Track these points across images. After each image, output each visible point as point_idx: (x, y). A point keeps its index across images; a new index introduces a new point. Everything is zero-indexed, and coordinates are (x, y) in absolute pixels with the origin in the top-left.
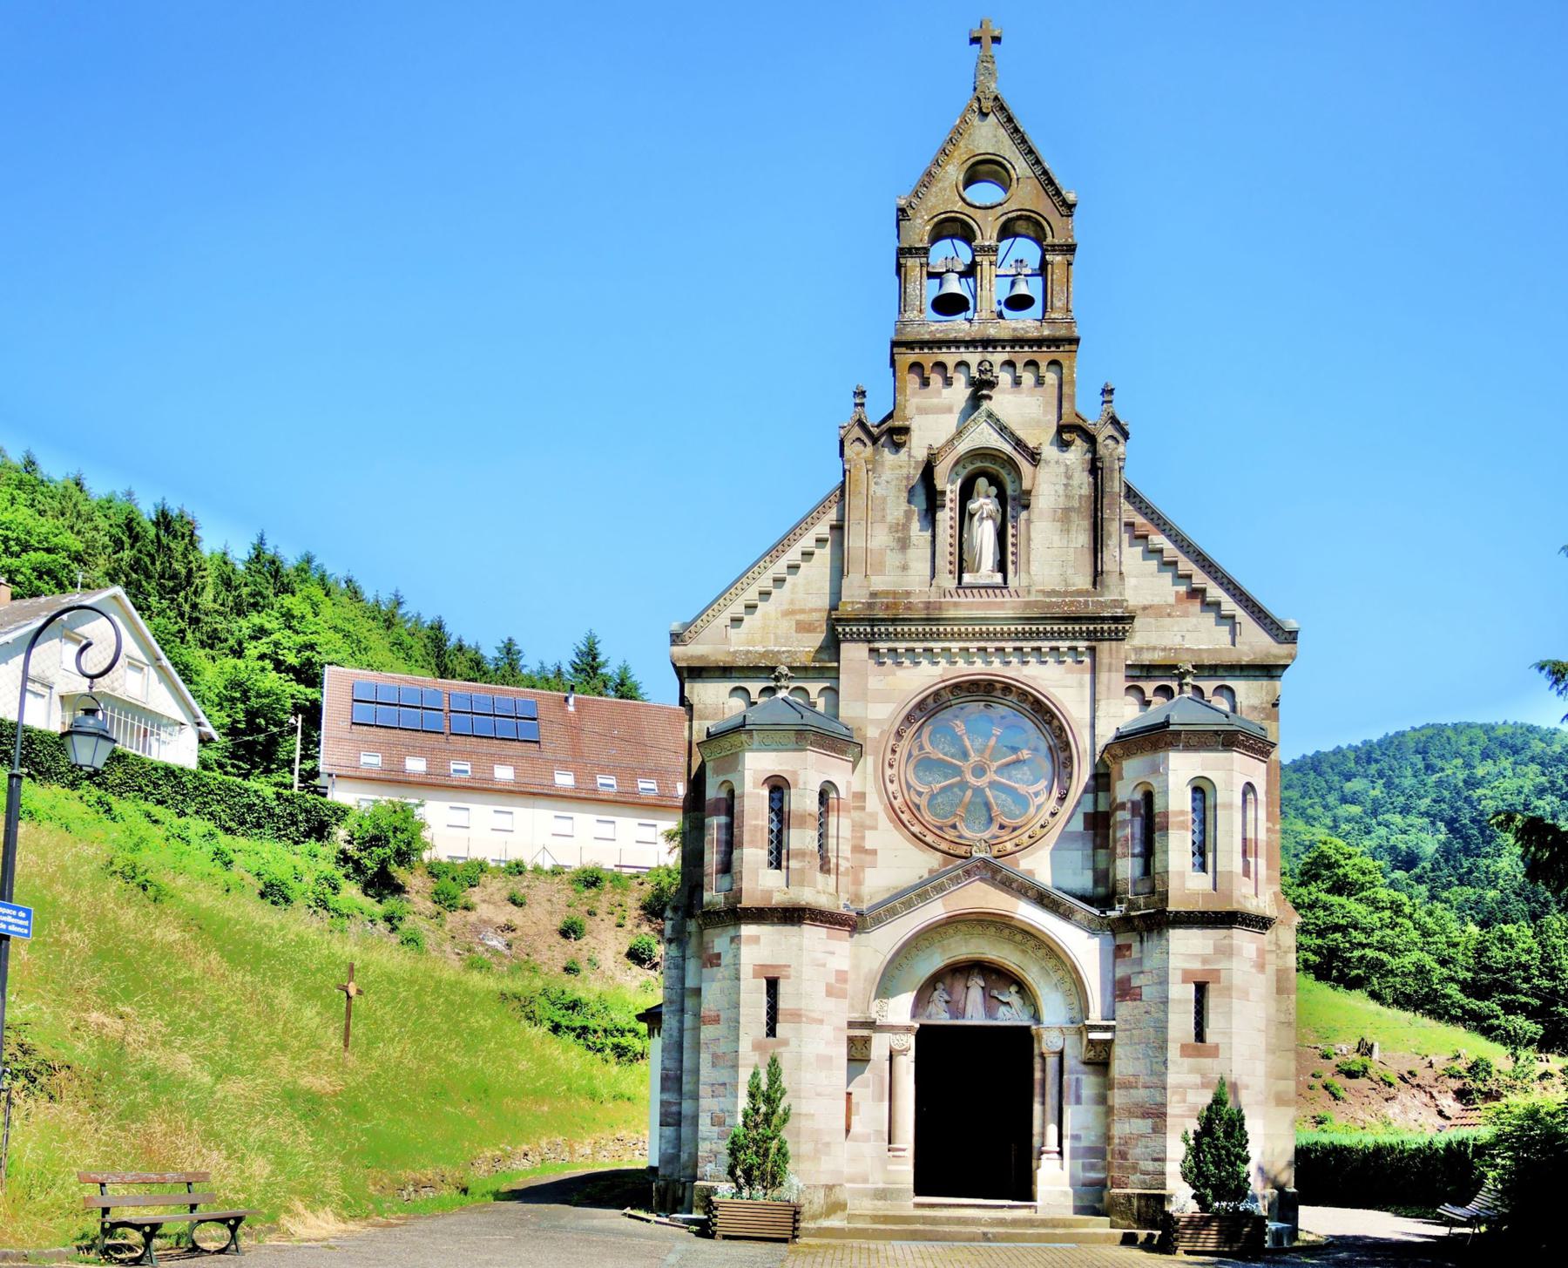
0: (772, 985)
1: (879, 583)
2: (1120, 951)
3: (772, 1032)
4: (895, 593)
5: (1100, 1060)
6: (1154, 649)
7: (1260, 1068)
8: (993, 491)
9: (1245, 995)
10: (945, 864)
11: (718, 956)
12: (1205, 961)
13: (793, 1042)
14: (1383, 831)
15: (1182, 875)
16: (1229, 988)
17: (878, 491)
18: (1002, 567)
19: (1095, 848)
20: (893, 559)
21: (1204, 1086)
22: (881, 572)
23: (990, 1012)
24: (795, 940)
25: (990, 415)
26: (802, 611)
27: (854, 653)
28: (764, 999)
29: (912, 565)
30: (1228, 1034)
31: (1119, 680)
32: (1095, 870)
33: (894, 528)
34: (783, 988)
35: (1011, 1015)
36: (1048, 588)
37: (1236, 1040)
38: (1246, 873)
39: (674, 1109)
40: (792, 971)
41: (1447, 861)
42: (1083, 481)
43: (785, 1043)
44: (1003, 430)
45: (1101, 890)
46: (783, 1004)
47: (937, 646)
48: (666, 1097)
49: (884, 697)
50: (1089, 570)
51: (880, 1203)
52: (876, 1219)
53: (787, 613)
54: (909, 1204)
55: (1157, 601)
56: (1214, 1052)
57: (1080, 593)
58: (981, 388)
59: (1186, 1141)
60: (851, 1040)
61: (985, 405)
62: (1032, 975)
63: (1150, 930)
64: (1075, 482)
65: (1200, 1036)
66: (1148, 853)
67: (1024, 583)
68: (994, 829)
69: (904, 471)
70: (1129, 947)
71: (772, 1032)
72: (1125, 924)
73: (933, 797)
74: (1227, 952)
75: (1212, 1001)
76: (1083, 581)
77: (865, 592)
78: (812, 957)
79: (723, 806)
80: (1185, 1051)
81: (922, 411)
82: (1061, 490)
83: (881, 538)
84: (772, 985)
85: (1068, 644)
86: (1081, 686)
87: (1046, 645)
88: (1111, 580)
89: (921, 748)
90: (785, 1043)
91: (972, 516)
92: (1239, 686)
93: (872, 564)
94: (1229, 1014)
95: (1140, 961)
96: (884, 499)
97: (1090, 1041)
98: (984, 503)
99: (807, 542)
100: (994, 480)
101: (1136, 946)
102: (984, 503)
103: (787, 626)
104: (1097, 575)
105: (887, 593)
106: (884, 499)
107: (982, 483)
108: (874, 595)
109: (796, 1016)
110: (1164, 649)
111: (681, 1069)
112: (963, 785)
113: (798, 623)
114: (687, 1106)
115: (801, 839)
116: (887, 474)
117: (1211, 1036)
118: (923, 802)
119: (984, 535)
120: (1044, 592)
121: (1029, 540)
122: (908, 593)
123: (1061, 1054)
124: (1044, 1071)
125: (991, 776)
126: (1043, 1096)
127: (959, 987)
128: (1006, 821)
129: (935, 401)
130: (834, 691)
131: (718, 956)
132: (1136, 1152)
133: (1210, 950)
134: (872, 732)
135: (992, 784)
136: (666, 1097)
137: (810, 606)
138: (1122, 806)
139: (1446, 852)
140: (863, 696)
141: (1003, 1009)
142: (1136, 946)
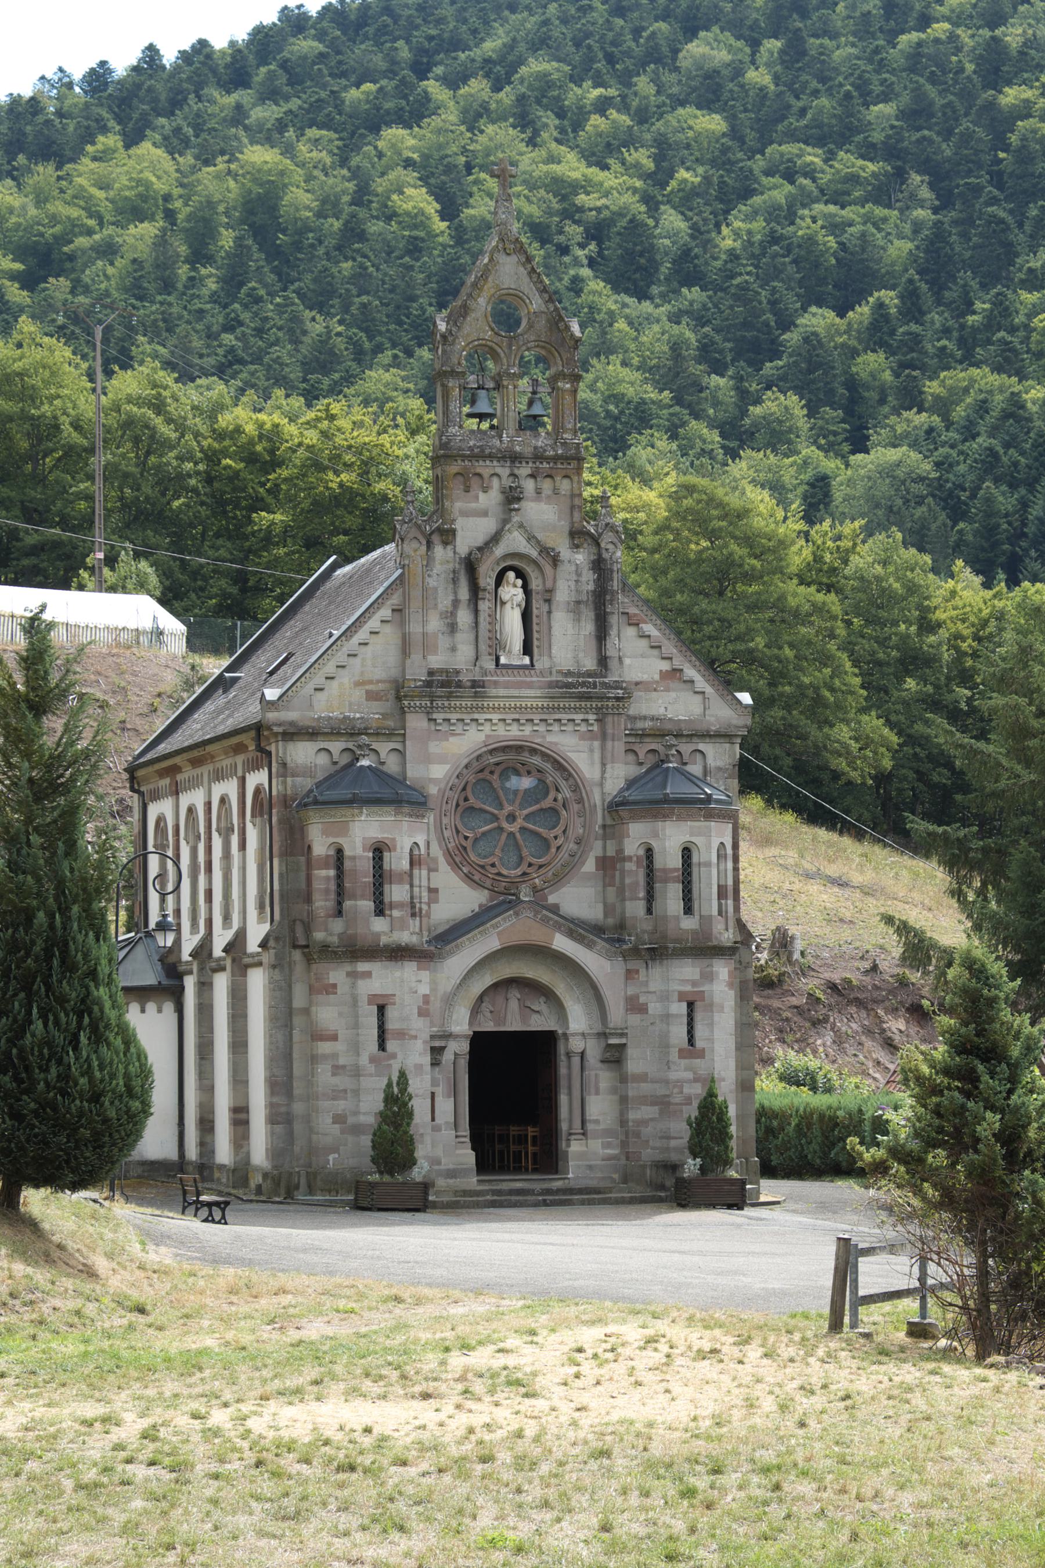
0: (381, 1009)
1: (437, 661)
2: (630, 974)
3: (382, 1046)
4: (447, 671)
5: (615, 1057)
6: (645, 718)
7: (732, 1063)
8: (519, 582)
9: (721, 1009)
10: (491, 899)
11: (335, 986)
12: (694, 984)
13: (400, 1056)
14: (779, 192)
15: (677, 918)
16: (711, 1005)
17: (432, 582)
18: (527, 649)
19: (605, 886)
20: (443, 642)
21: (696, 1080)
22: (435, 653)
23: (524, 1019)
24: (398, 974)
25: (521, 526)
26: (370, 682)
27: (416, 723)
28: (374, 1021)
29: (459, 646)
30: (711, 1040)
31: (620, 746)
32: (605, 905)
33: (444, 615)
34: (391, 1013)
35: (540, 1022)
36: (565, 669)
37: (716, 1046)
38: (720, 913)
39: (283, 1109)
40: (397, 999)
41: (938, 287)
42: (589, 578)
43: (394, 1056)
44: (531, 538)
45: (610, 921)
46: (391, 1025)
47: (481, 717)
48: (275, 1100)
49: (442, 760)
50: (594, 653)
51: (451, 1181)
52: (456, 1193)
53: (358, 684)
54: (472, 1182)
55: (645, 677)
56: (701, 1054)
57: (589, 674)
58: (512, 498)
59: (690, 1124)
60: (433, 1049)
61: (516, 519)
62: (561, 989)
63: (653, 959)
64: (584, 579)
65: (691, 1041)
66: (650, 897)
67: (547, 665)
68: (524, 867)
69: (451, 566)
70: (637, 972)
71: (382, 1046)
72: (635, 952)
73: (476, 840)
74: (708, 977)
75: (698, 1016)
76: (590, 664)
77: (425, 671)
78: (405, 984)
79: (332, 861)
80: (682, 1054)
81: (466, 514)
82: (572, 584)
83: (435, 624)
84: (381, 1009)
85: (581, 716)
86: (591, 751)
87: (564, 717)
88: (613, 664)
89: (466, 799)
90: (394, 1056)
91: (503, 603)
92: (708, 748)
93: (428, 646)
94: (711, 1025)
95: (646, 984)
96: (436, 589)
97: (609, 1046)
98: (512, 592)
99: (373, 623)
100: (520, 574)
101: (643, 972)
102: (512, 592)
103: (359, 694)
104: (603, 661)
105: (441, 671)
106: (436, 589)
107: (511, 575)
108: (431, 673)
109: (401, 1035)
110: (652, 719)
111: (290, 1076)
112: (501, 829)
113: (367, 692)
114: (298, 1108)
115: (396, 893)
116: (438, 568)
117: (699, 1044)
118: (468, 844)
119: (512, 622)
120: (559, 672)
121: (550, 628)
122: (457, 672)
123: (582, 1054)
124: (569, 1067)
125: (520, 822)
126: (570, 1088)
127: (500, 999)
128: (534, 860)
129: (474, 505)
130: (401, 753)
131: (335, 986)
132: (647, 1131)
133: (697, 977)
134: (433, 790)
135: (523, 829)
136: (275, 1100)
137: (376, 677)
138: (630, 858)
139: (935, 263)
140: (428, 759)
141: (535, 1016)
142: (643, 972)
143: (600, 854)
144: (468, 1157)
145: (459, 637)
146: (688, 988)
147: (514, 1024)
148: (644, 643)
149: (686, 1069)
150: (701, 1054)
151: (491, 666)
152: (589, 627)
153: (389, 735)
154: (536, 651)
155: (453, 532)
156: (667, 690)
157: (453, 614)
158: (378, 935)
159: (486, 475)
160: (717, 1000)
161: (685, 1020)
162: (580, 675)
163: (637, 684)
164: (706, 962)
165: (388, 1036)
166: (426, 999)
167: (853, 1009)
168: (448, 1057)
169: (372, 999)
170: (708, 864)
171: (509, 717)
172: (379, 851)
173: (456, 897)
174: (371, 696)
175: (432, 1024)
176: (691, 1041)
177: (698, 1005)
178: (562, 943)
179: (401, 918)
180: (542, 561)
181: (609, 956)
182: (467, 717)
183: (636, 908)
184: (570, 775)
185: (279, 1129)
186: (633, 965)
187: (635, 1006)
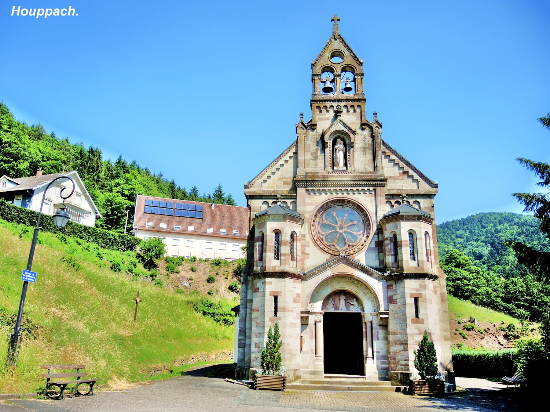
0: (276, 298)
1: (308, 170)
2: (389, 287)
3: (276, 315)
5: (384, 325)
8: (342, 142)
9: (431, 302)
10: (331, 258)
11: (258, 288)
15: (407, 261)
16: (425, 299)
17: (308, 142)
18: (346, 165)
19: (379, 253)
20: (312, 162)
21: (420, 334)
23: (347, 308)
24: (283, 283)
26: (285, 178)
28: (273, 303)
30: (426, 315)
31: (384, 199)
32: (379, 260)
35: (354, 309)
38: (428, 261)
39: (243, 342)
40: (282, 294)
41: (492, 257)
42: (369, 140)
43: (280, 318)
44: (344, 125)
47: (327, 189)
49: (311, 204)
50: (372, 166)
51: (313, 376)
53: (280, 179)
54: (322, 376)
55: (393, 175)
56: (422, 322)
57: (370, 173)
58: (338, 113)
61: (339, 118)
62: (361, 295)
63: (398, 280)
64: (367, 140)
65: (417, 316)
66: (396, 254)
67: (353, 169)
70: (392, 285)
71: (276, 315)
72: (390, 278)
73: (327, 236)
75: (420, 304)
76: (371, 169)
77: (304, 172)
79: (260, 239)
83: (309, 156)
84: (276, 298)
85: (367, 188)
86: (372, 201)
88: (379, 168)
89: (323, 220)
93: (306, 164)
94: (426, 308)
95: (396, 290)
96: (309, 145)
97: (381, 318)
98: (340, 146)
99: (286, 157)
100: (342, 139)
101: (394, 285)
102: (340, 146)
103: (280, 183)
104: (375, 167)
105: (311, 173)
106: (309, 145)
107: (339, 140)
108: (307, 173)
112: (336, 232)
113: (284, 182)
114: (247, 341)
115: (285, 249)
117: (421, 316)
118: (324, 237)
119: (340, 155)
121: (354, 157)
122: (317, 173)
123: (371, 322)
124: (366, 328)
125: (345, 229)
126: (366, 337)
127: (337, 299)
128: (350, 244)
131: (258, 288)
134: (307, 216)
135: (345, 232)
137: (287, 176)
138: (387, 239)
139: (491, 254)
140: (304, 204)
141: (352, 307)
143: (377, 240)
144: (320, 364)
145: (318, 161)
146: (414, 292)
147: (343, 309)
148: (392, 164)
149: (415, 328)
150: (422, 322)
151: (331, 170)
152: (370, 156)
153: (290, 197)
154: (348, 165)
155: (315, 125)
156: (403, 179)
157: (316, 153)
158: (275, 267)
159: (328, 107)
160: (428, 297)
161: (414, 306)
162: (366, 173)
163: (390, 177)
164: (422, 280)
165: (278, 310)
166: (298, 295)
167: (490, 335)
168: (312, 319)
169: (272, 293)
170: (421, 239)
171: (338, 189)
172: (278, 233)
173: (315, 257)
174: (285, 183)
175: (302, 306)
176: (417, 316)
177: (420, 300)
178: (358, 274)
179: (285, 260)
180: (349, 133)
181: (380, 279)
182: (321, 189)
183: (389, 259)
184: (364, 210)
185: (241, 350)
186: (389, 283)
187: (390, 300)
